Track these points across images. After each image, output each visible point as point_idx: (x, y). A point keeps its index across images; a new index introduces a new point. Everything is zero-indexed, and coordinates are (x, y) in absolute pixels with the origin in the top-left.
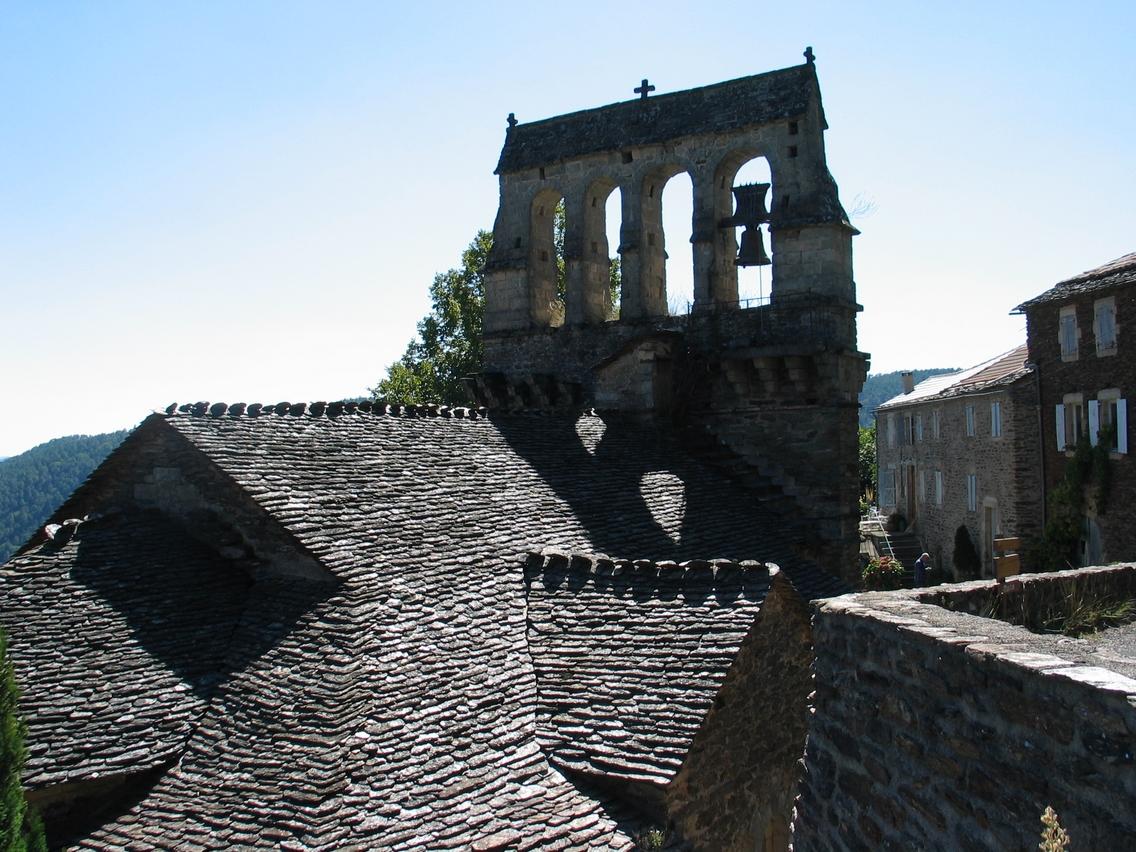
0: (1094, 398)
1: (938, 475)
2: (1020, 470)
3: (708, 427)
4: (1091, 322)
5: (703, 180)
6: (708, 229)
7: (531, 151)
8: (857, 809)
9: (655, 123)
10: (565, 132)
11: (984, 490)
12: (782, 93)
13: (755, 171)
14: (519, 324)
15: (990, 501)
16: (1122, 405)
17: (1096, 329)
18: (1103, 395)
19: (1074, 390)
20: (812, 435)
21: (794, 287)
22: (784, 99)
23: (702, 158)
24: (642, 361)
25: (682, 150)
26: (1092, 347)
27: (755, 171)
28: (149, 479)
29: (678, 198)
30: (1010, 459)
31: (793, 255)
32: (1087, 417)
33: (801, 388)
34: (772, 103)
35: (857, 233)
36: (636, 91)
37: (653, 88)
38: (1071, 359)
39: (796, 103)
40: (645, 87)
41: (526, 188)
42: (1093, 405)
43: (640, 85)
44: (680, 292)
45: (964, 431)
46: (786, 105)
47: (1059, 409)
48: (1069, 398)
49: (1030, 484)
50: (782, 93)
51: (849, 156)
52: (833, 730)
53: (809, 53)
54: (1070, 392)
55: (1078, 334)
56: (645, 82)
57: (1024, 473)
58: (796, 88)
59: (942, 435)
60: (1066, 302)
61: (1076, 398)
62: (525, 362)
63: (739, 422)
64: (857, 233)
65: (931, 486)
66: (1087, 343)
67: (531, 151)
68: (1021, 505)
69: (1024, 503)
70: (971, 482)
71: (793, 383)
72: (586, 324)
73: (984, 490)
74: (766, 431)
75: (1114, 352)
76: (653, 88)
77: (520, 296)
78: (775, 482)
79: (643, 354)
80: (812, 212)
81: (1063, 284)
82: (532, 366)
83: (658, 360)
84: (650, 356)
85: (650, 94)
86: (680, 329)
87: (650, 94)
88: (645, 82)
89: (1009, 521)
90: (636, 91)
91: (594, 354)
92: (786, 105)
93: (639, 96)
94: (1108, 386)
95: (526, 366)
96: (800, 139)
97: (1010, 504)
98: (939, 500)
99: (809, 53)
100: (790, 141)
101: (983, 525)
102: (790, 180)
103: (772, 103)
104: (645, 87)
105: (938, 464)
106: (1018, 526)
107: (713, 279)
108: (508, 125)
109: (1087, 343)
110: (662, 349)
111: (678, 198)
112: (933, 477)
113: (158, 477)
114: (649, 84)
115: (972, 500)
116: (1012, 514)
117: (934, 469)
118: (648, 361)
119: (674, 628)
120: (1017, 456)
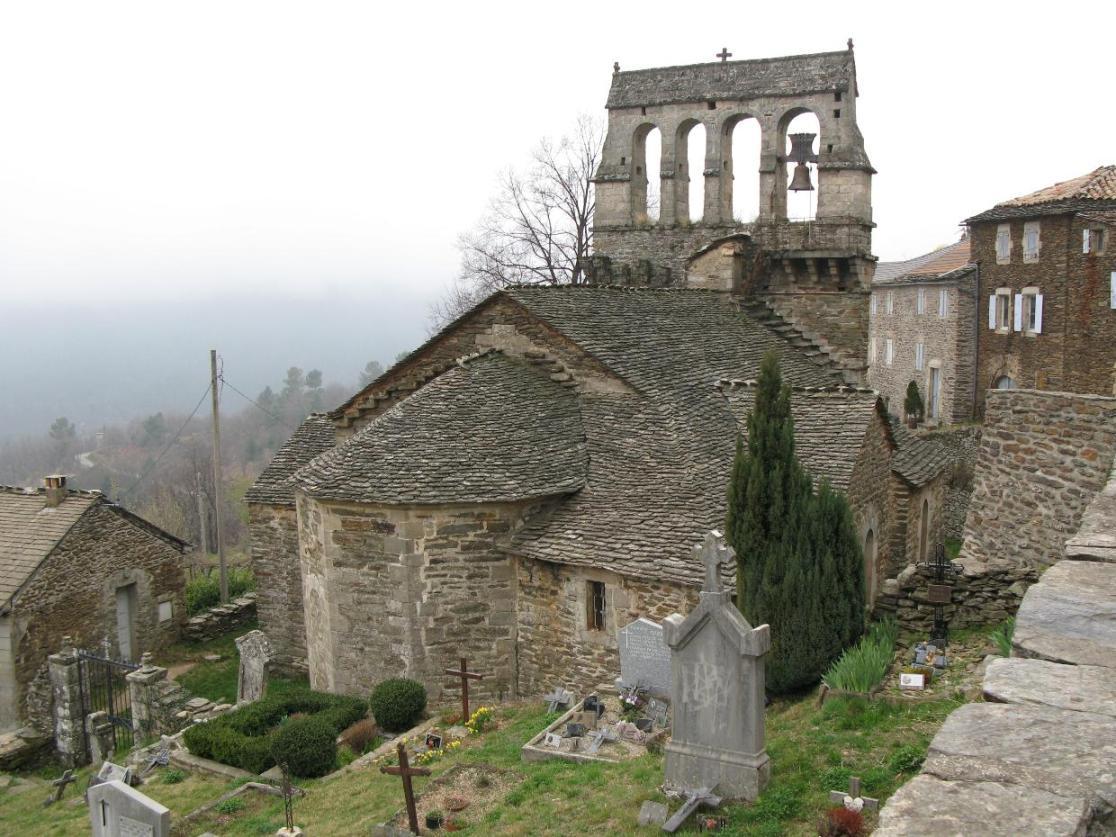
0: (1019, 292)
1: (889, 342)
2: (961, 343)
3: (768, 303)
4: (1021, 237)
5: (769, 128)
6: (772, 165)
7: (636, 95)
8: (1013, 455)
9: (733, 83)
10: (660, 81)
11: (929, 356)
12: (830, 70)
13: (805, 123)
14: (623, 222)
15: (935, 363)
16: (1039, 299)
17: (1025, 243)
18: (1027, 290)
19: (1004, 285)
20: (841, 312)
21: (834, 209)
22: (832, 75)
23: (769, 113)
24: (724, 256)
25: (754, 106)
26: (1020, 256)
27: (805, 123)
28: (489, 331)
29: (748, 139)
30: (952, 334)
31: (833, 187)
32: (1013, 305)
33: (836, 280)
34: (823, 77)
35: (875, 172)
36: (719, 55)
37: (730, 55)
38: (1003, 263)
39: (840, 79)
40: (725, 54)
41: (630, 121)
42: (1018, 298)
43: (728, 52)
44: (747, 206)
45: (916, 310)
46: (832, 79)
47: (993, 299)
48: (1000, 291)
49: (967, 352)
50: (830, 70)
51: (868, 113)
52: (999, 433)
53: (850, 45)
54: (1000, 287)
55: (1010, 245)
56: (725, 50)
57: (963, 344)
58: (840, 67)
59: (894, 311)
60: (1003, 222)
61: (1007, 291)
62: (628, 250)
63: (789, 301)
64: (875, 172)
65: (882, 349)
66: (1017, 252)
67: (636, 95)
68: (959, 367)
69: (961, 366)
70: (919, 350)
71: (831, 276)
72: (676, 224)
73: (929, 356)
74: (809, 308)
75: (1037, 261)
76: (730, 55)
77: (623, 201)
78: (814, 343)
79: (726, 251)
80: (848, 160)
81: (1012, 217)
82: (633, 253)
83: (736, 255)
84: (731, 252)
85: (728, 59)
86: (748, 233)
87: (728, 59)
88: (725, 50)
89: (950, 378)
90: (719, 55)
91: (682, 247)
92: (832, 79)
93: (720, 60)
94: (1030, 285)
95: (627, 253)
96: (841, 105)
97: (952, 365)
98: (889, 360)
99: (850, 45)
100: (836, 106)
101: (928, 380)
102: (834, 134)
103: (823, 77)
104: (725, 54)
105: (890, 333)
106: (957, 382)
107: (774, 201)
108: (613, 70)
109: (1017, 252)
110: (739, 247)
111: (748, 139)
112: (885, 344)
113: (496, 330)
114: (728, 52)
115: (919, 363)
116: (952, 373)
117: (886, 337)
118: (729, 256)
119: (823, 423)
120: (958, 332)
